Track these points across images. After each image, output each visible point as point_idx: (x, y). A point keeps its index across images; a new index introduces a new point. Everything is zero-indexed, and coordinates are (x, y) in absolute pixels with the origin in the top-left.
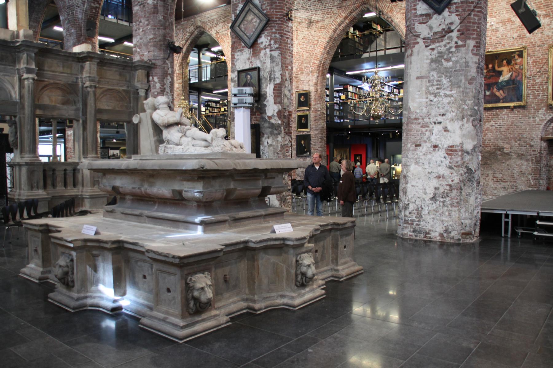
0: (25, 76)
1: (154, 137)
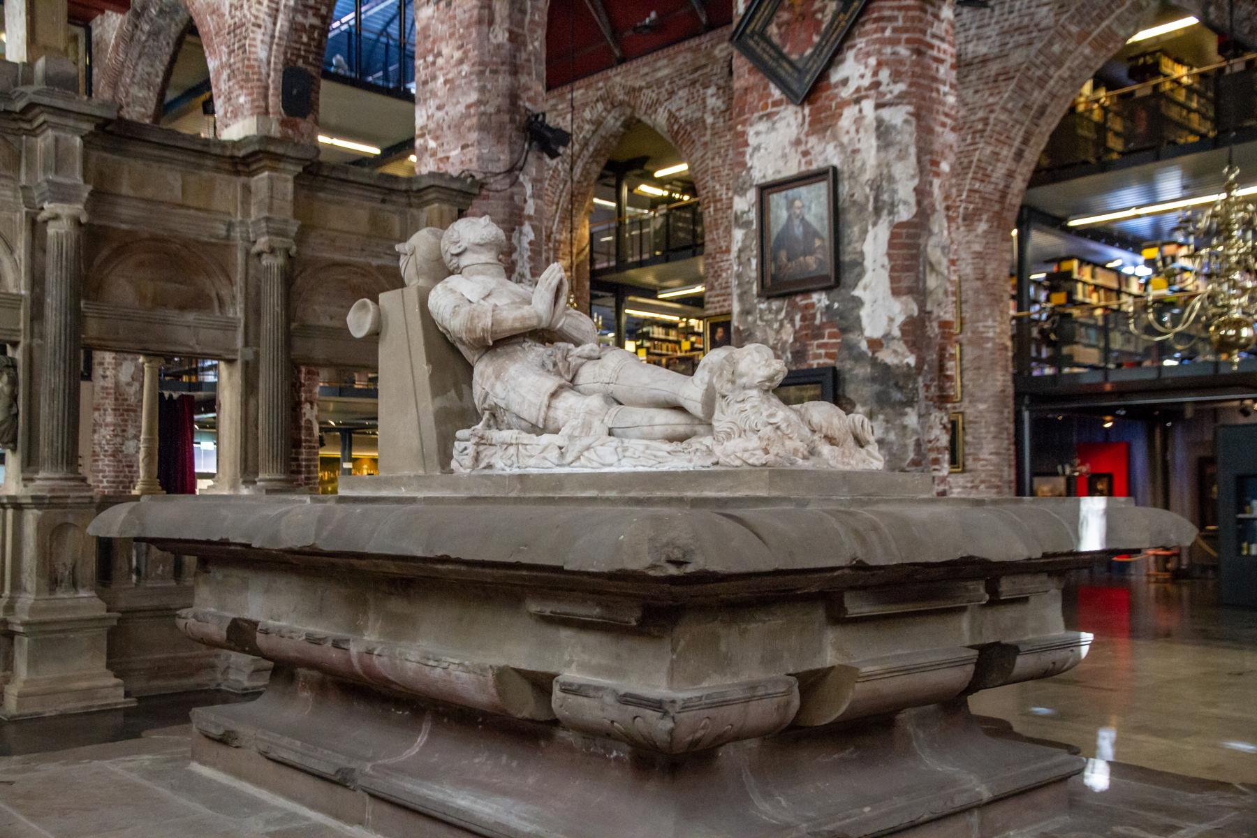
0: (49, 208)
1: (435, 394)
